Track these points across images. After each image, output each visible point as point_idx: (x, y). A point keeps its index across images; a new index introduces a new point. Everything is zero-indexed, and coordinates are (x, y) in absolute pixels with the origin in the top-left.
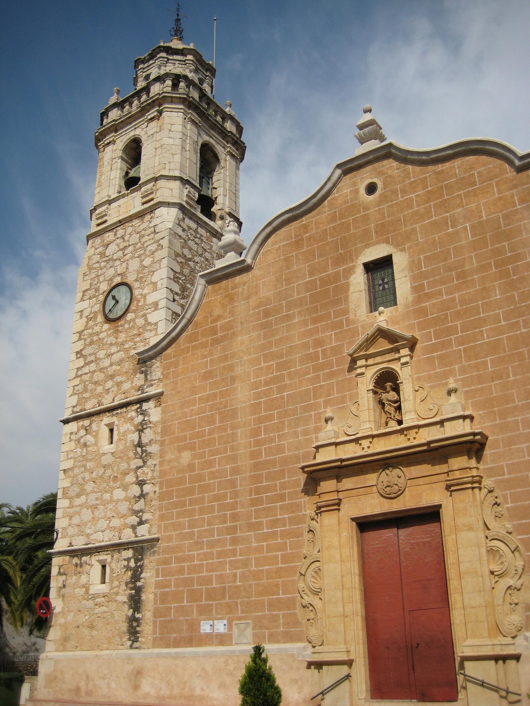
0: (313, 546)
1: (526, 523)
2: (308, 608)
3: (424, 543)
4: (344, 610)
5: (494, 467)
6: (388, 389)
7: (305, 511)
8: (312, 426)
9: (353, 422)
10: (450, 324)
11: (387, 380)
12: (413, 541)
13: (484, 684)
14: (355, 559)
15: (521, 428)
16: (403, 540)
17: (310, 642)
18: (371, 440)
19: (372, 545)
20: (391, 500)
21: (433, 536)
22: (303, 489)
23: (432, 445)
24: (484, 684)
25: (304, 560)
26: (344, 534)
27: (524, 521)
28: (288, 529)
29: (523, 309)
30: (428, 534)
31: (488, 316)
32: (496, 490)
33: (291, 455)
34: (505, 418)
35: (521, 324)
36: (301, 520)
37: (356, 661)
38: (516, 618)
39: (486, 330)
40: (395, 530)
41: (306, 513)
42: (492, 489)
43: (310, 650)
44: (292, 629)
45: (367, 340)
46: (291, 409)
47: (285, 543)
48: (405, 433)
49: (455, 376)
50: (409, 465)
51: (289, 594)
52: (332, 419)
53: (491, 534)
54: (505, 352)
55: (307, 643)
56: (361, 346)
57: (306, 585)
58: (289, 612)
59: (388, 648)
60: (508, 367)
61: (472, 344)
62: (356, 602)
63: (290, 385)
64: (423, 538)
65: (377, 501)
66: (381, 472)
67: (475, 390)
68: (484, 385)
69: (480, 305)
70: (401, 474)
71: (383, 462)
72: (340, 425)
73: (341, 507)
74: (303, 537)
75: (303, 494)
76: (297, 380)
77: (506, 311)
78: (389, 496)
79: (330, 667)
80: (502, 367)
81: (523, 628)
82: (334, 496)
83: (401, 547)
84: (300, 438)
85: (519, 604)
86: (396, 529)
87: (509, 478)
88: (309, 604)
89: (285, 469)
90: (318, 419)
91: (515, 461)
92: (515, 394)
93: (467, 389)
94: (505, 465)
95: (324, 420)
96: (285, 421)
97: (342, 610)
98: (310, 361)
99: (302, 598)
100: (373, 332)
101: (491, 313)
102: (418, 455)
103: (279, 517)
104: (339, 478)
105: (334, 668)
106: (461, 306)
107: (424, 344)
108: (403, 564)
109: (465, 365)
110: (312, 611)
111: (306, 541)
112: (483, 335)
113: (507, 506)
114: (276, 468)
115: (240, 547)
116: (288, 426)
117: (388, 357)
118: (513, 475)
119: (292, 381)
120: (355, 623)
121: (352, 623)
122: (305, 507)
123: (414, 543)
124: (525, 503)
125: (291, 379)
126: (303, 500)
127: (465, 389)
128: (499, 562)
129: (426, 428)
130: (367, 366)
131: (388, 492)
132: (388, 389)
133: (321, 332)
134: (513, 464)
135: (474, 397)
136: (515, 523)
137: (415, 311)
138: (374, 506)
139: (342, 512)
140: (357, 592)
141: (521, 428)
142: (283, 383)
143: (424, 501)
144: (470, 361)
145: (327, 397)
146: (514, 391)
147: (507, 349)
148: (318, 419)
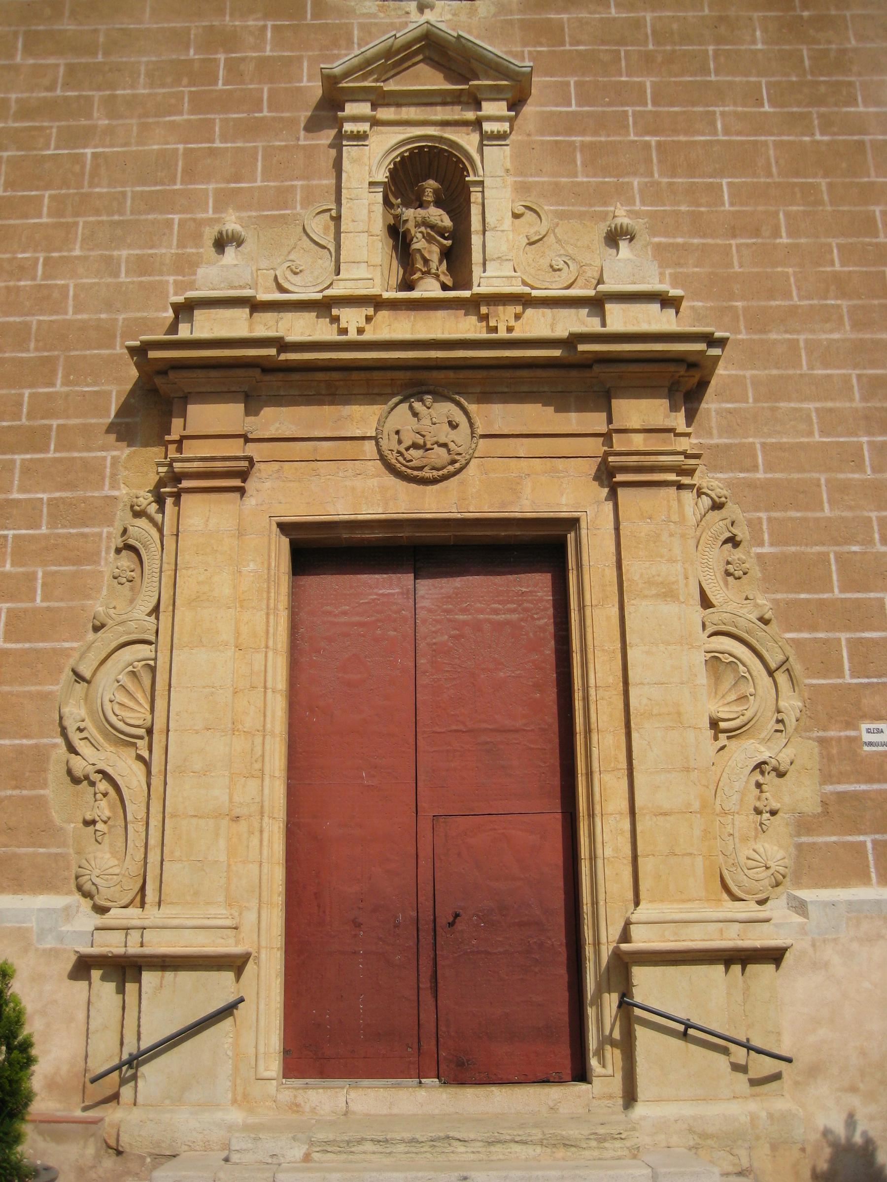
0: (129, 594)
1: (808, 600)
2: (93, 784)
3: (498, 626)
4: (231, 801)
5: (728, 447)
6: (429, 196)
7: (113, 487)
8: (168, 250)
9: (317, 255)
10: (624, 79)
11: (430, 178)
12: (461, 617)
13: (691, 1031)
14: (279, 646)
15: (804, 363)
16: (430, 611)
17: (87, 895)
18: (370, 311)
19: (330, 613)
20: (421, 488)
21: (526, 610)
22: (112, 424)
23: (581, 348)
24: (691, 1031)
25: (91, 636)
26: (252, 566)
27: (803, 596)
28: (46, 537)
29: (823, 89)
30: (512, 602)
31: (730, 83)
32: (730, 504)
33: (82, 321)
34: (763, 331)
35: (816, 122)
36: (102, 511)
37: (257, 958)
38: (775, 850)
39: (723, 114)
40: (408, 579)
41: (115, 493)
42: (723, 499)
43: (87, 920)
44: (23, 850)
45: (388, 53)
46: (101, 196)
47: (31, 578)
48: (484, 310)
49: (630, 201)
50: (486, 397)
51: (27, 736)
52: (238, 241)
53: (715, 618)
54: (770, 174)
55: (77, 897)
56: (368, 62)
57: (91, 712)
58: (16, 792)
59: (357, 925)
60: (777, 213)
61: (683, 138)
62: (272, 777)
63: (109, 131)
64: (496, 612)
65: (374, 482)
66: (397, 405)
67: (684, 247)
68: (709, 241)
69: (711, 53)
70: (459, 416)
71: (408, 374)
72: (264, 264)
73: (251, 485)
74: (97, 563)
75: (113, 437)
76: (134, 121)
77: (779, 83)
78: (416, 473)
79: (169, 975)
80: (760, 208)
81: (788, 879)
82: (234, 448)
83: (422, 630)
84: (123, 278)
85: (780, 814)
86: (411, 576)
87: (767, 479)
88: (100, 772)
89: (57, 358)
90: (190, 235)
91: (785, 440)
92: (792, 280)
93: (663, 240)
94: (758, 446)
95: (210, 243)
96: (76, 224)
97: (226, 798)
98: (185, 81)
99: (72, 749)
100: (410, 36)
101: (738, 79)
102: (524, 373)
103: (15, 495)
104: (253, 402)
105: (185, 978)
106: (657, 43)
107: (548, 109)
108: (423, 680)
109: (659, 183)
110: (105, 795)
111: (107, 576)
112: (713, 124)
113: (759, 550)
114: (28, 351)
115: (529, 49)
116: (83, 240)
117: (440, 113)
118: (778, 475)
119: (115, 122)
120: (265, 843)
121: (255, 841)
122: (113, 475)
123: (465, 623)
124: (809, 550)
125: (112, 114)
126: (109, 455)
127: (656, 240)
128: (733, 697)
129: (548, 312)
130: (375, 123)
131: (414, 464)
132: (429, 196)
133: (231, 15)
134: (781, 447)
135: (679, 265)
136: (779, 596)
137: (526, 26)
138: (360, 495)
139: (251, 501)
140: (277, 746)
141: (804, 363)
142: (83, 122)
143: (527, 503)
144: (674, 175)
145: (229, 182)
146: (790, 270)
147: (774, 170)
148: (190, 235)
